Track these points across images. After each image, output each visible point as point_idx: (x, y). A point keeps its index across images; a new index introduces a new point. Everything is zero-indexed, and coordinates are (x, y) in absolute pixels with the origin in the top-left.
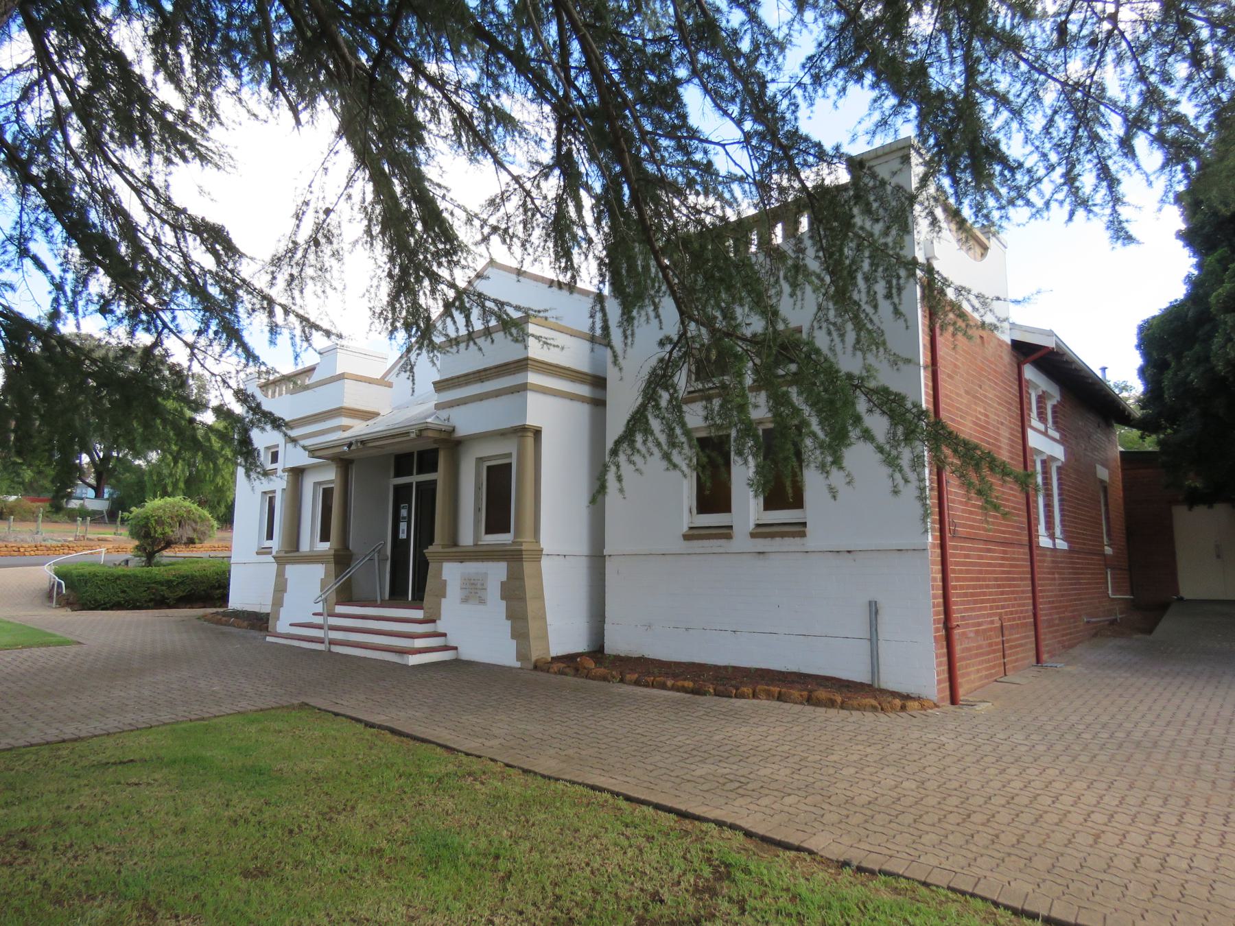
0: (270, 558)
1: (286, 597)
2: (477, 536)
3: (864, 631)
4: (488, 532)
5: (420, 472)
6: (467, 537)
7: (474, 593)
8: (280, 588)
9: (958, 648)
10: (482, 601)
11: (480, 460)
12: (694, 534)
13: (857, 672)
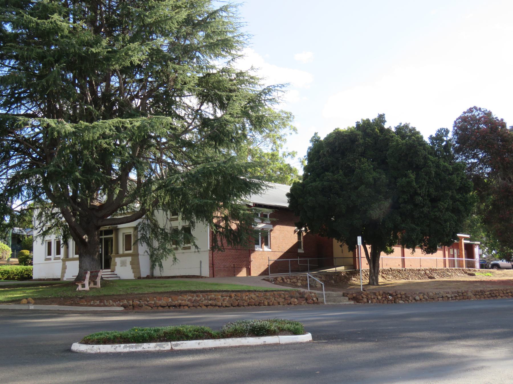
0: (61, 261)
1: (67, 270)
2: (123, 252)
3: (199, 266)
4: (126, 250)
5: (105, 235)
6: (121, 251)
7: (123, 264)
8: (64, 268)
9: (215, 269)
10: (126, 266)
11: (123, 233)
12: (46, 259)
13: (198, 274)
